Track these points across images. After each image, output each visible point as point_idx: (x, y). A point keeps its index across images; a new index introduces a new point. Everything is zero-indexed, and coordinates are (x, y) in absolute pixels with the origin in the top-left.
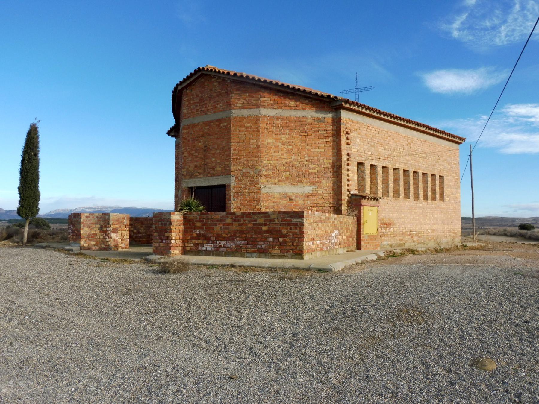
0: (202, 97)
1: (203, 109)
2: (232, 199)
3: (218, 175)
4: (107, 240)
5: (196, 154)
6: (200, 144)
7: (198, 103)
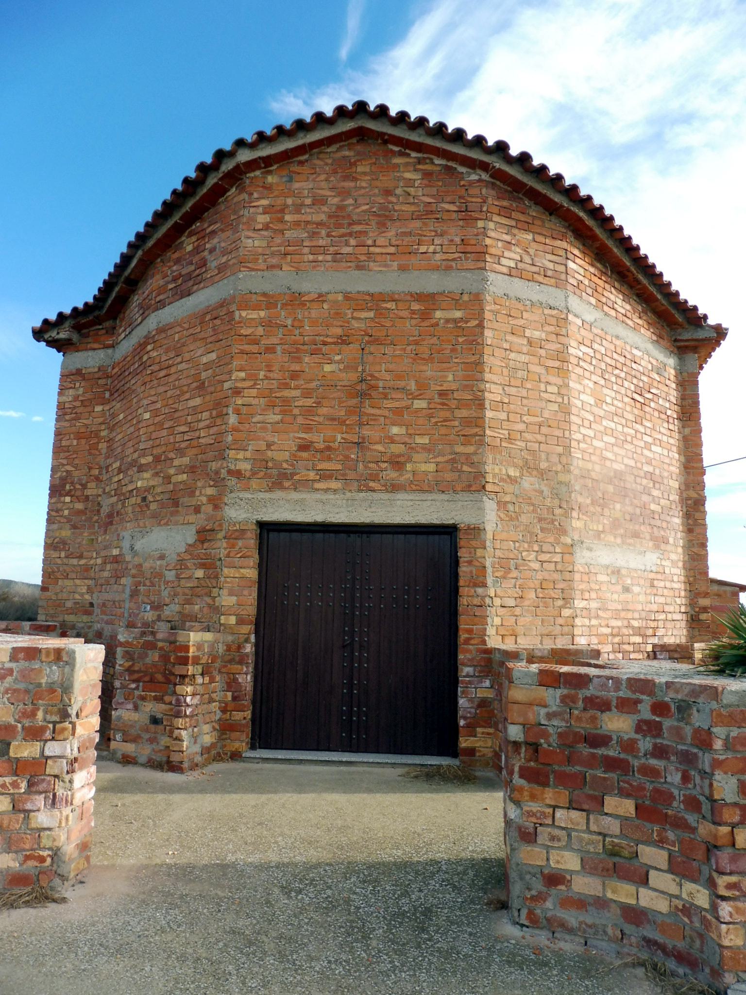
0: (341, 208)
1: (346, 250)
2: (490, 581)
3: (419, 486)
4: (43, 818)
5: (309, 402)
6: (327, 368)
7: (320, 224)
